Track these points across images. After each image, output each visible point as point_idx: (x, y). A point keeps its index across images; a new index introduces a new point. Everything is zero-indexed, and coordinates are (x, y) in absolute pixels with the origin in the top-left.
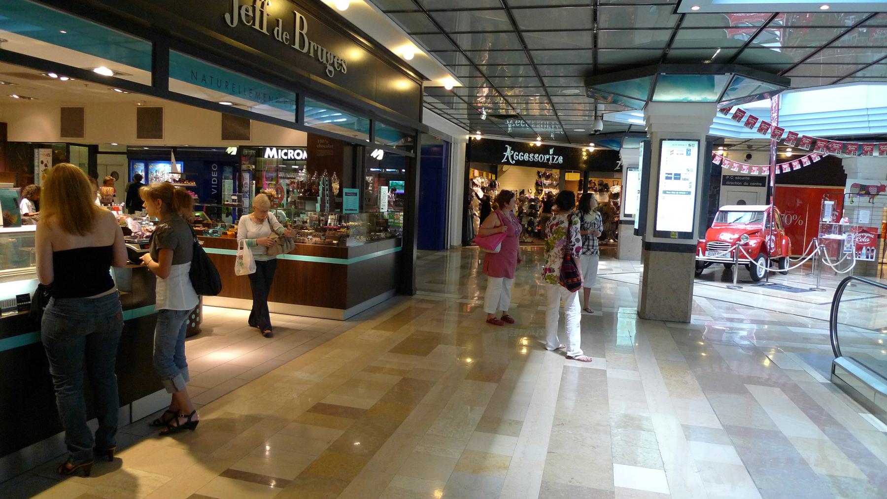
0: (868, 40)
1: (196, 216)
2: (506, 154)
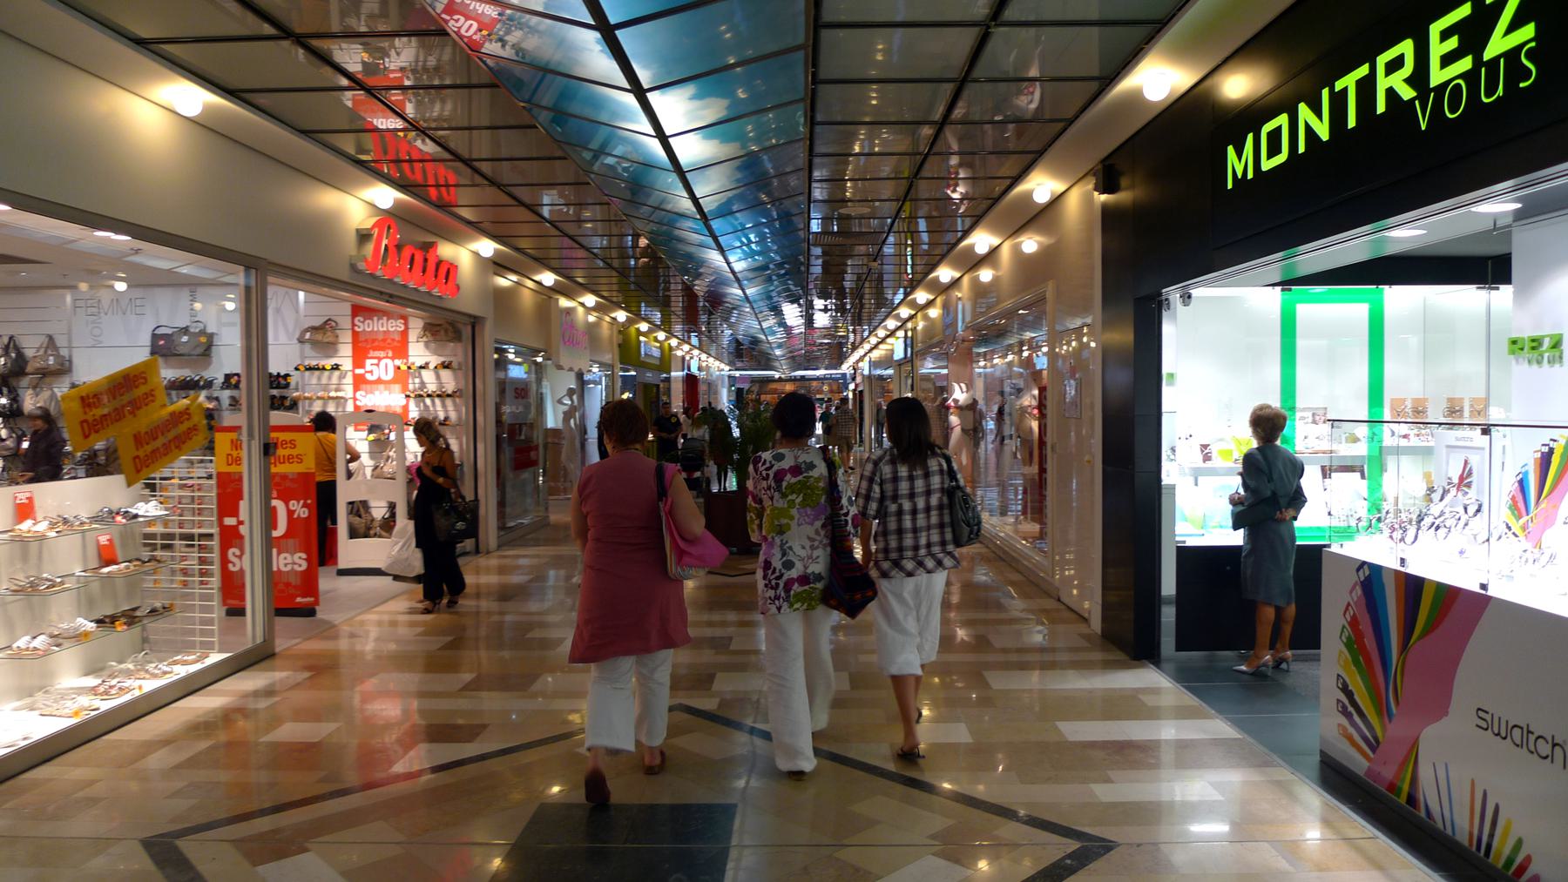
0: (1432, 434)
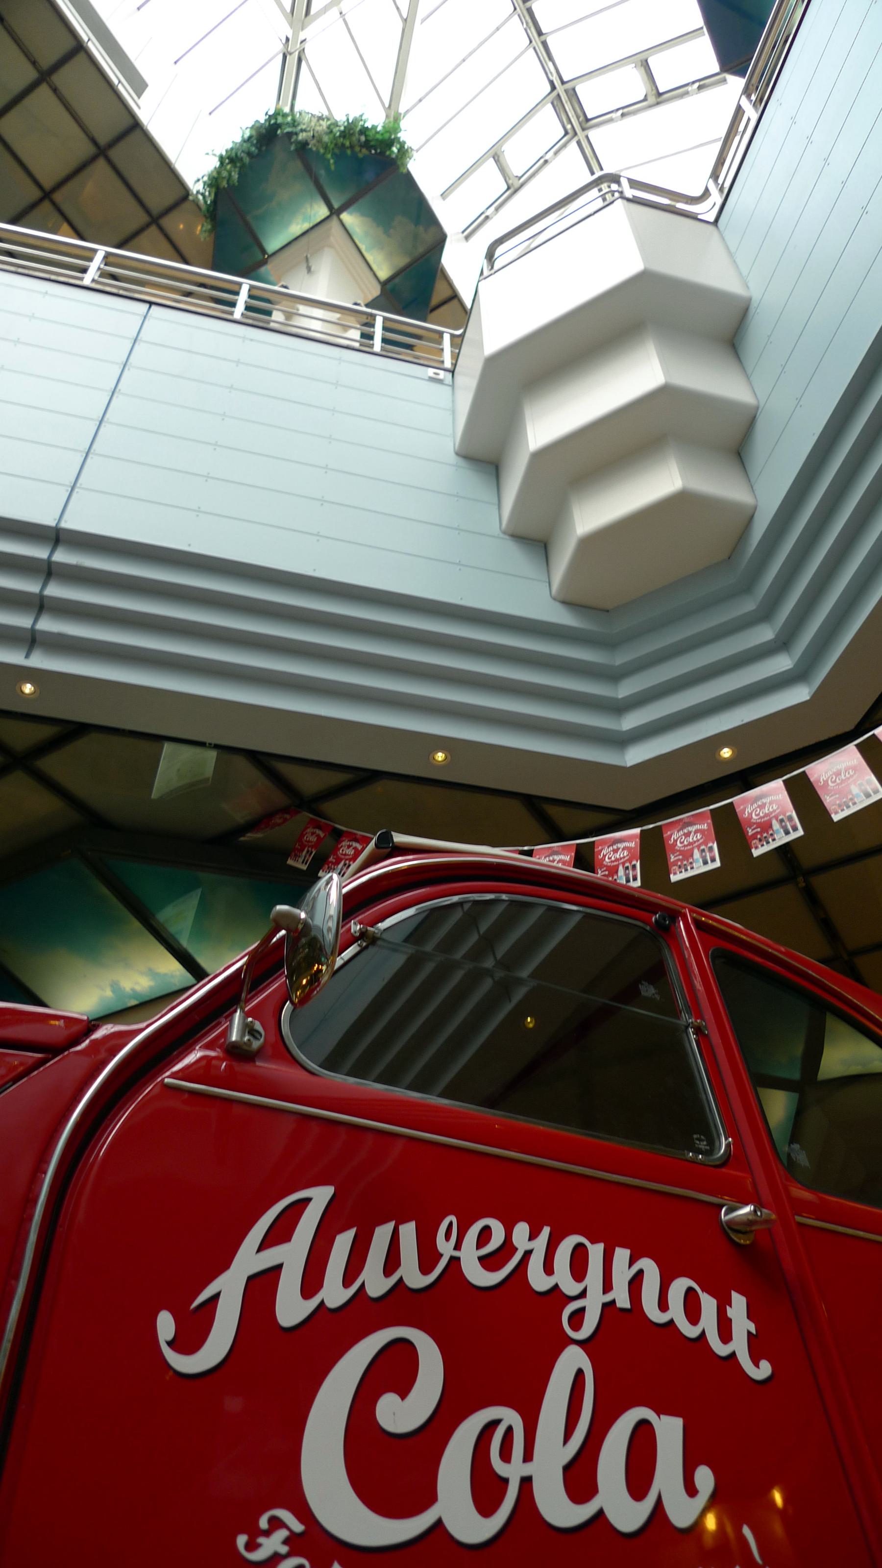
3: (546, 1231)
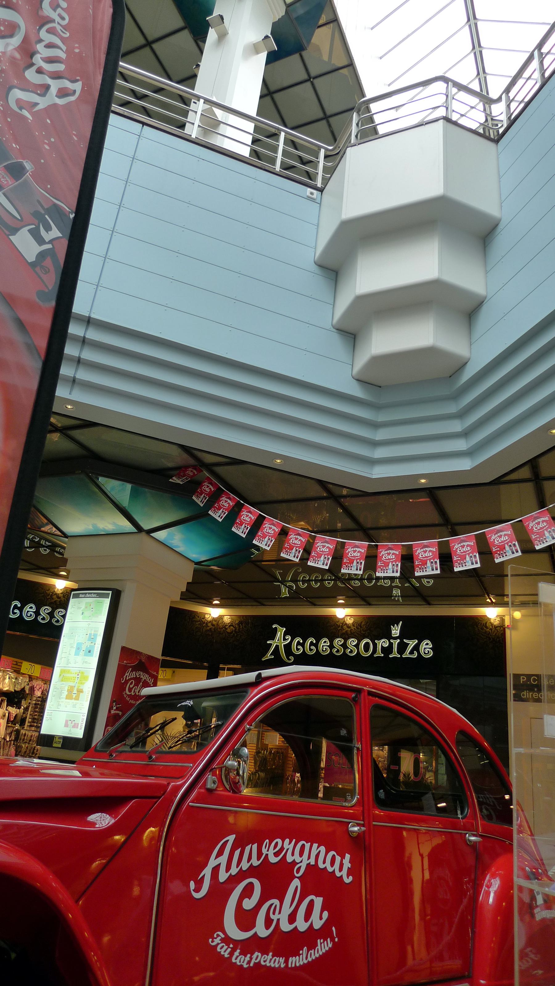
1: (89, 6)
2: (274, 643)
3: (294, 840)
